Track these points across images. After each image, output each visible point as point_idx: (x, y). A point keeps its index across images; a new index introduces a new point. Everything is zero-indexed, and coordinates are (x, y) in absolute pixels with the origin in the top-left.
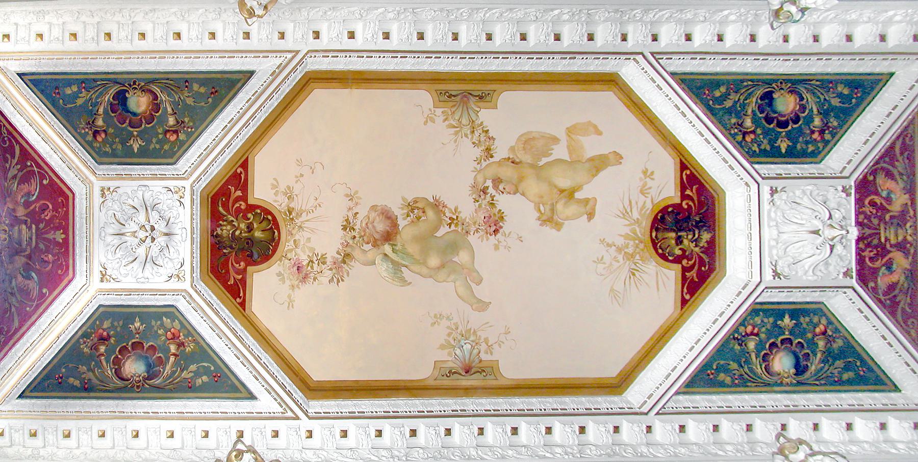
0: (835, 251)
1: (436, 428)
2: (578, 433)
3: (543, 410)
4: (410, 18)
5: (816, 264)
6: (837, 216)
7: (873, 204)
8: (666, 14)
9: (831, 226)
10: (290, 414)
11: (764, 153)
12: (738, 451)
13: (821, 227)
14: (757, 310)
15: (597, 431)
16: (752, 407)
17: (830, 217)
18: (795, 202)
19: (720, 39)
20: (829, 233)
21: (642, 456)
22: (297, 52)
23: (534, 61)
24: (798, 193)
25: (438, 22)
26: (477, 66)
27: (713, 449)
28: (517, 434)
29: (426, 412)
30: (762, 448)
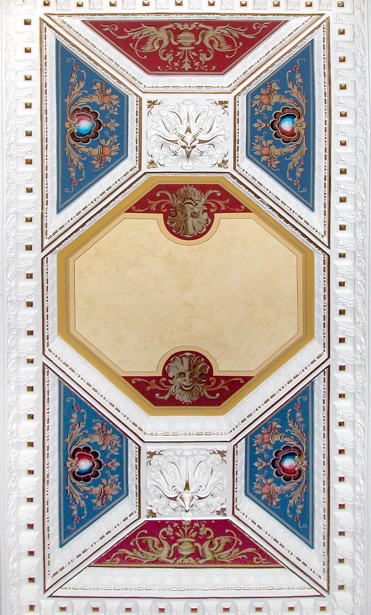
0: (172, 501)
1: (33, 180)
3: (48, 411)
4: (358, 219)
6: (201, 504)
7: (208, 533)
8: (361, 573)
10: (46, 242)
12: (12, 433)
13: (191, 491)
14: (123, 437)
16: (48, 474)
17: (200, 498)
18: (212, 470)
19: (342, 506)
20: (187, 495)
21: (9, 495)
22: (329, 247)
23: (322, 322)
24: (221, 474)
25: (355, 186)
26: (317, 411)
27: (14, 412)
28: (27, 278)
29: (47, 314)
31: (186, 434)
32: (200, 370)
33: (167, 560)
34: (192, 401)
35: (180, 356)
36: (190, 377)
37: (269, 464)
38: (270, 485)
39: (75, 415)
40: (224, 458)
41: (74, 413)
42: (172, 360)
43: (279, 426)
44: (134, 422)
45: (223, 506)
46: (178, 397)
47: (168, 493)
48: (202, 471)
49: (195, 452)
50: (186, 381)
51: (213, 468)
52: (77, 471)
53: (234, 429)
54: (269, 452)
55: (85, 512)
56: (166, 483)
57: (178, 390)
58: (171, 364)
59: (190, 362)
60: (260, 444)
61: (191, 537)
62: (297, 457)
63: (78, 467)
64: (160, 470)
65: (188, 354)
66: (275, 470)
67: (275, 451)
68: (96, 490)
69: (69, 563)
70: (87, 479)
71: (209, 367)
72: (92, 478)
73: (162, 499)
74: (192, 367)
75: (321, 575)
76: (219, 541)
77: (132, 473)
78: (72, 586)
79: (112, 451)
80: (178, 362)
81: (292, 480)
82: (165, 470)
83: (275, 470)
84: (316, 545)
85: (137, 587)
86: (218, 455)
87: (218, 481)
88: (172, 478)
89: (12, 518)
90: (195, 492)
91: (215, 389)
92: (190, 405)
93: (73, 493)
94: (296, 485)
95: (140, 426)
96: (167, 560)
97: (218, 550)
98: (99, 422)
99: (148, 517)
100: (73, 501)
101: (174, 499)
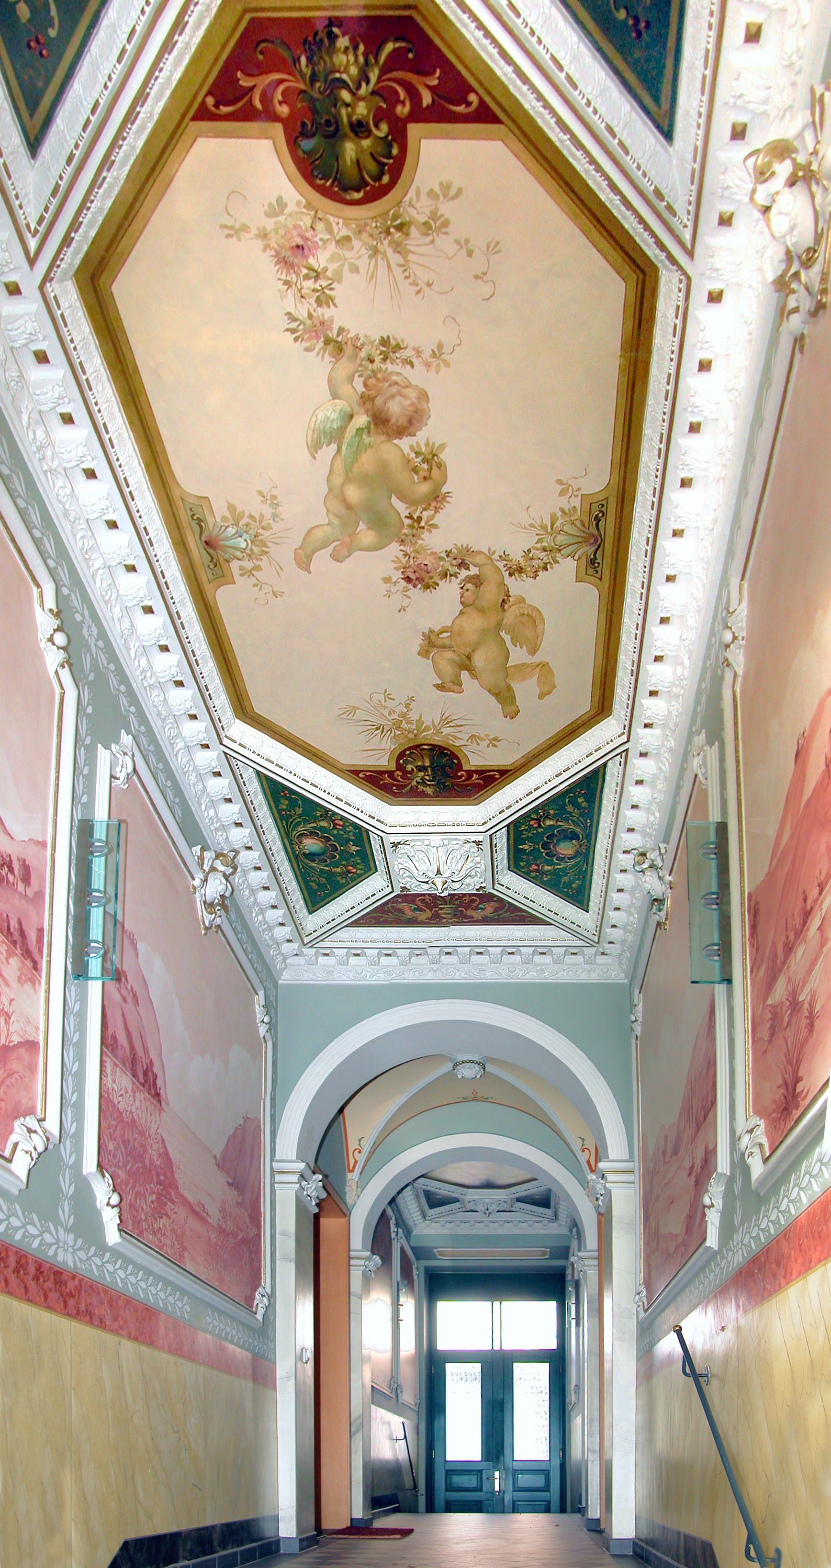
17: (453, 881)
22: (690, 254)
49: (446, 842)
86: (474, 844)
101: (427, 883)
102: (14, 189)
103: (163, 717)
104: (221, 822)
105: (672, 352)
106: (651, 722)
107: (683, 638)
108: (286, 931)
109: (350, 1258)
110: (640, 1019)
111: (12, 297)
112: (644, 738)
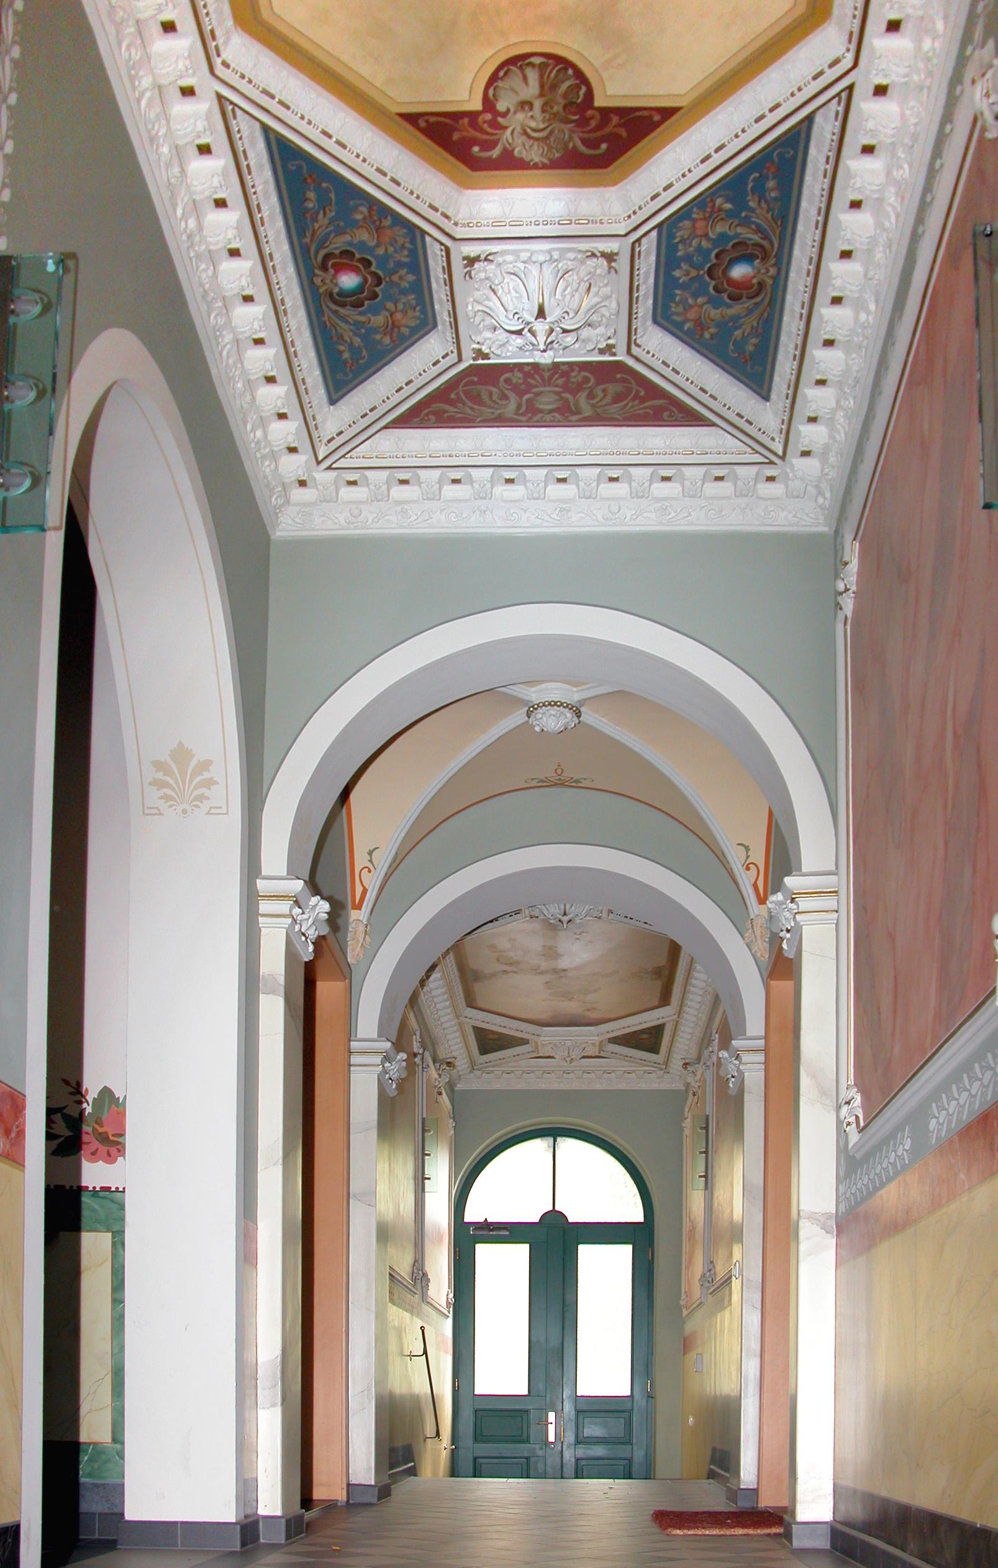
0: (514, 336)
2: (229, 246)
3: (253, 190)
5: (492, 314)
6: (569, 339)
7: (586, 380)
9: (552, 331)
11: (672, 248)
12: (190, 236)
13: (548, 320)
14: (415, 234)
15: (276, 396)
17: (565, 331)
24: (606, 291)
30: (269, 466)
31: (537, 223)
32: (565, 95)
33: (516, 417)
34: (550, 160)
35: (519, 64)
36: (543, 111)
37: (701, 272)
38: (701, 306)
39: (311, 195)
40: (613, 264)
41: (309, 190)
42: (501, 74)
43: (728, 206)
44: (432, 203)
45: (611, 342)
46: (520, 152)
47: (508, 324)
48: (569, 288)
49: (556, 255)
50: (535, 120)
51: (592, 281)
52: (336, 290)
53: (635, 213)
54: (703, 253)
55: (364, 353)
56: (502, 308)
57: (518, 138)
58: (500, 83)
59: (541, 76)
60: (688, 239)
61: (556, 386)
62: (758, 261)
63: (336, 284)
64: (491, 287)
65: (537, 60)
66: (713, 283)
67: (716, 251)
68: (379, 320)
69: (350, 426)
70: (358, 305)
71: (584, 89)
72: (366, 302)
73: (497, 332)
74: (547, 88)
75: (775, 436)
76: (604, 390)
77: (439, 292)
78: (361, 455)
79: (396, 255)
80: (514, 80)
81: (744, 300)
82: (499, 287)
83: (713, 283)
84: (773, 396)
85: (467, 453)
87: (601, 302)
88: (514, 299)
89: (233, 370)
90: (556, 321)
91: (599, 134)
92: (544, 167)
93: (336, 325)
94: (750, 307)
95: (444, 210)
96: (516, 417)
97: (603, 403)
98: (362, 205)
99: (474, 359)
100: (338, 339)
101: (519, 333)
102: (210, 24)
103: (209, 299)
104: (271, 446)
105: (834, 134)
106: (824, 378)
107: (869, 276)
108: (287, 431)
109: (350, 1065)
110: (854, 588)
111: (291, 454)
112: (809, 434)
